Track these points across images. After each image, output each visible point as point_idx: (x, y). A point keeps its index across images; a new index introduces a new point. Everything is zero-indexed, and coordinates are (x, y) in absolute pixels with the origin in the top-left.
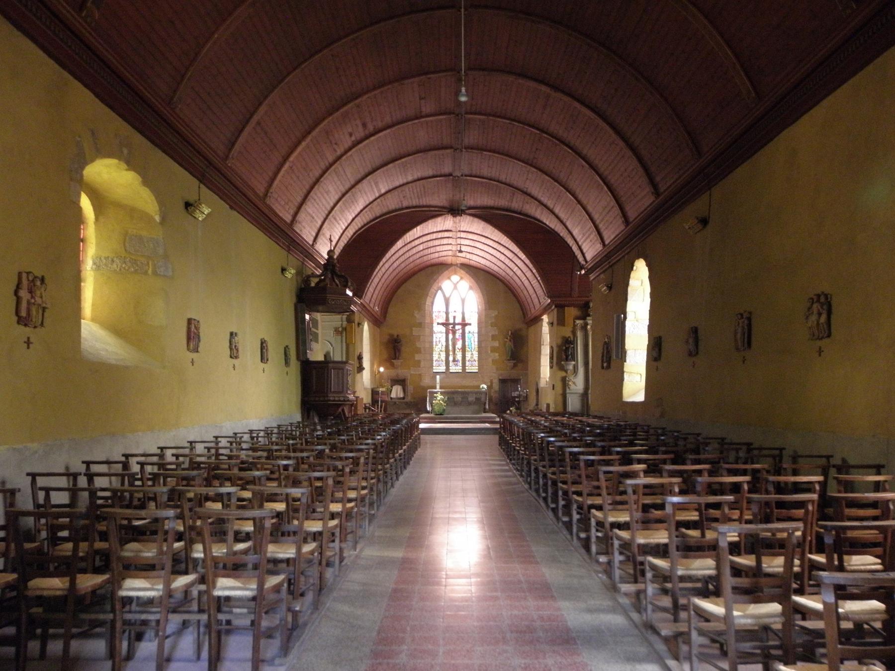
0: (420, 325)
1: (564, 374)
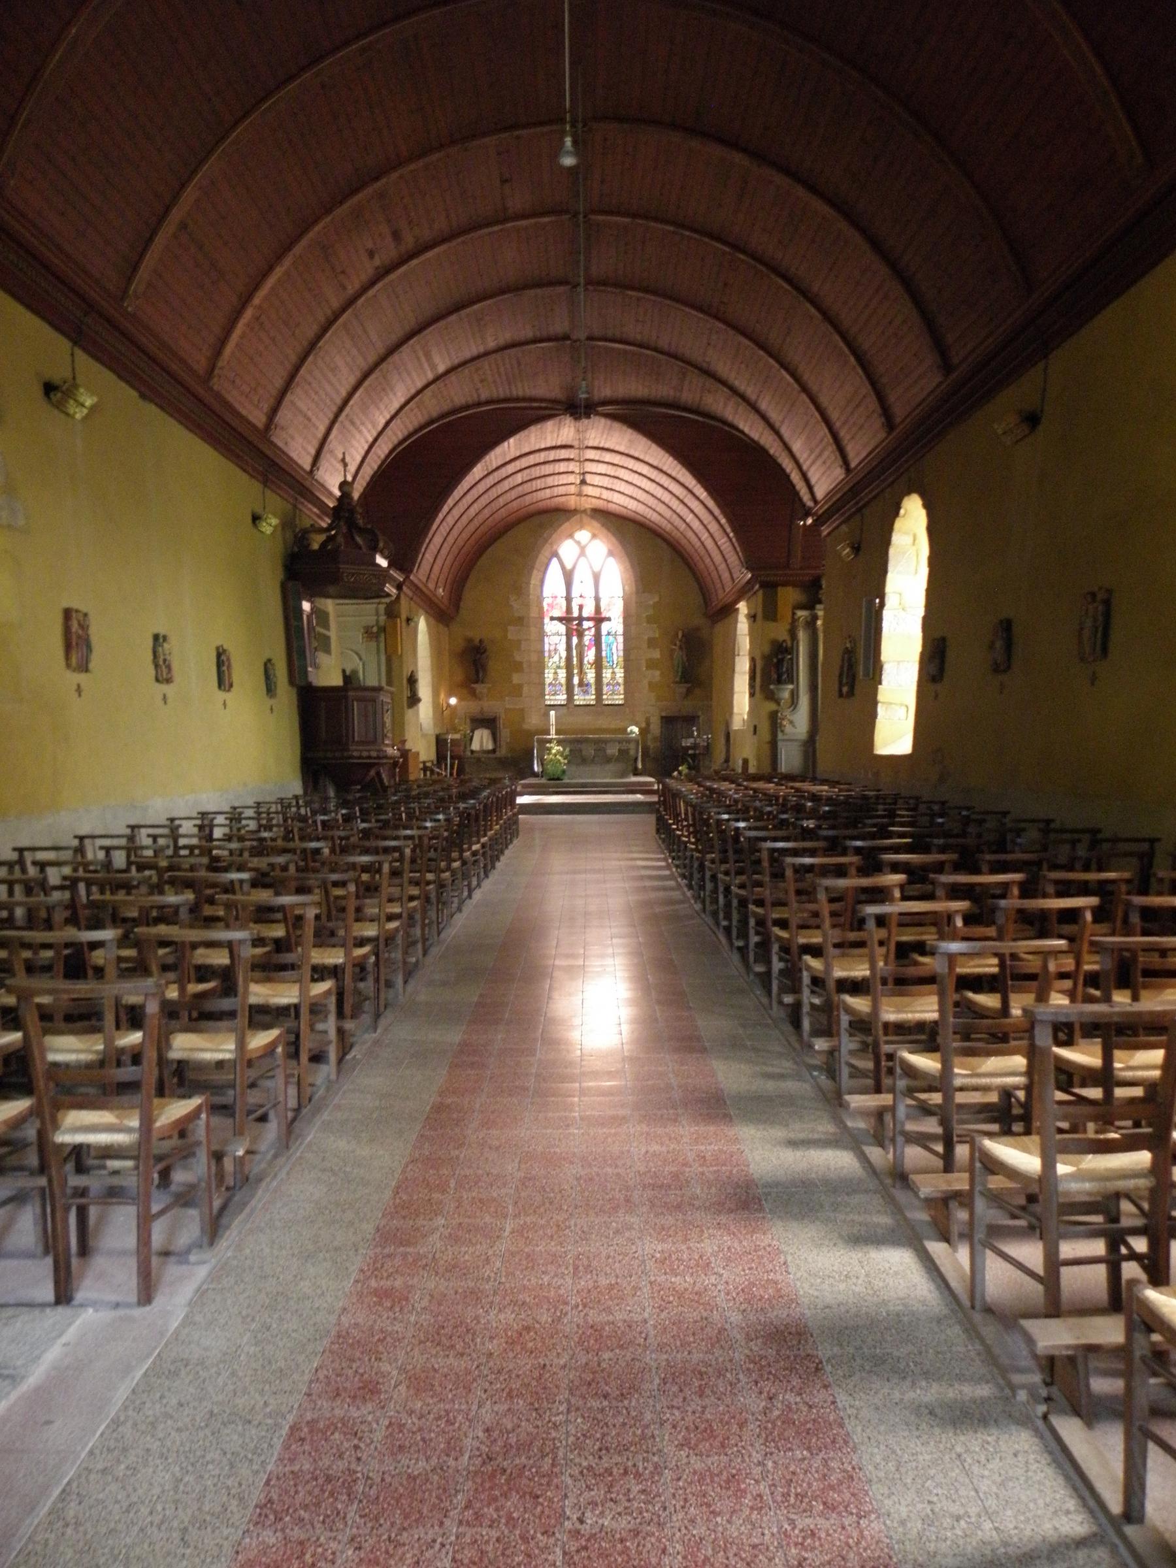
0: (520, 621)
1: (772, 706)
